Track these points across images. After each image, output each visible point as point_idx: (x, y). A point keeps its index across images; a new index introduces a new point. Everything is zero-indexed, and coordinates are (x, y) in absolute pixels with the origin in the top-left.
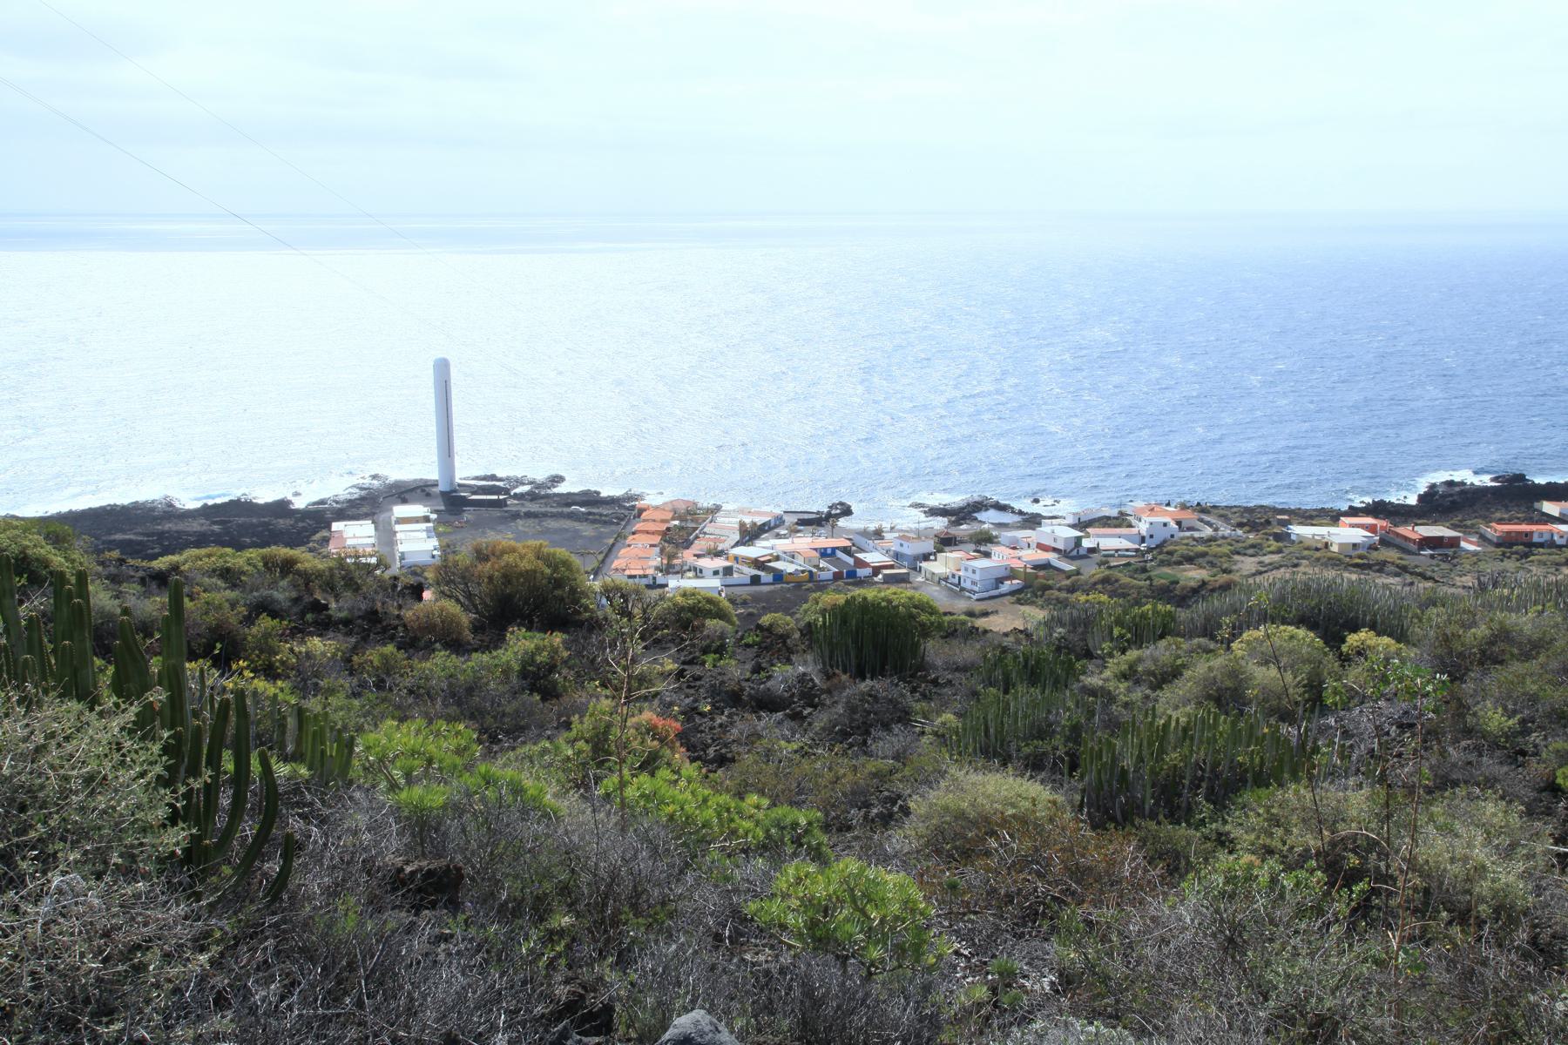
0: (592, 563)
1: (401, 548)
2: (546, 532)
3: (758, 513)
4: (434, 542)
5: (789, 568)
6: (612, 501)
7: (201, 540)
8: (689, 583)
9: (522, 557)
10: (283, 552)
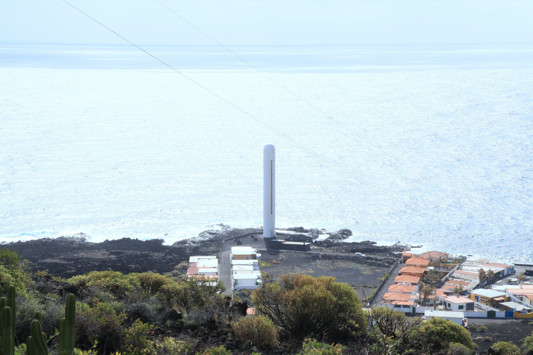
0: (370, 293)
1: (235, 276)
2: (338, 269)
3: (495, 265)
4: (258, 273)
5: (519, 308)
6: (384, 250)
7: (102, 266)
8: (440, 314)
9: (317, 288)
10: (154, 276)
